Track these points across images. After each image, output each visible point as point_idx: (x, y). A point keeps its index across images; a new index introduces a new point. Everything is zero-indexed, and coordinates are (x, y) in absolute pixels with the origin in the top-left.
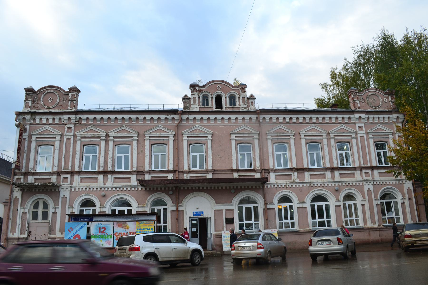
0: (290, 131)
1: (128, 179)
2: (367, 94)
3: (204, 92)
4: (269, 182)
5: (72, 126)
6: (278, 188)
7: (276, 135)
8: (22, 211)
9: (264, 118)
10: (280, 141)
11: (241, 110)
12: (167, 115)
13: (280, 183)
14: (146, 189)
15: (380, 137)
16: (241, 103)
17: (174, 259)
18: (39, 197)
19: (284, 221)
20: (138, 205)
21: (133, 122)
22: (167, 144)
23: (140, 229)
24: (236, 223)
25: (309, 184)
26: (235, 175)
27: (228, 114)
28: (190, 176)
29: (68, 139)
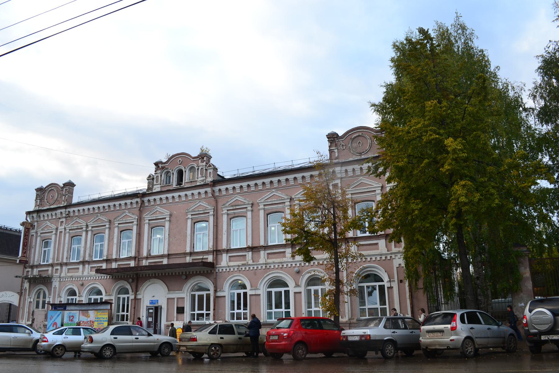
0: (247, 202)
1: (282, 254)
2: (350, 137)
3: (166, 169)
4: (221, 265)
5: (64, 220)
6: (230, 272)
7: (232, 208)
8: (29, 300)
9: (220, 190)
10: (236, 215)
11: (198, 184)
12: (131, 199)
13: (232, 266)
14: (112, 277)
15: (362, 195)
16: (200, 175)
17: (11, 347)
18: (40, 288)
19: (236, 311)
20: (251, 288)
21: (106, 210)
22: (283, 212)
23: (97, 318)
24: (186, 312)
25: (265, 266)
26: (188, 259)
27: (188, 189)
28: (149, 263)
29: (61, 232)
